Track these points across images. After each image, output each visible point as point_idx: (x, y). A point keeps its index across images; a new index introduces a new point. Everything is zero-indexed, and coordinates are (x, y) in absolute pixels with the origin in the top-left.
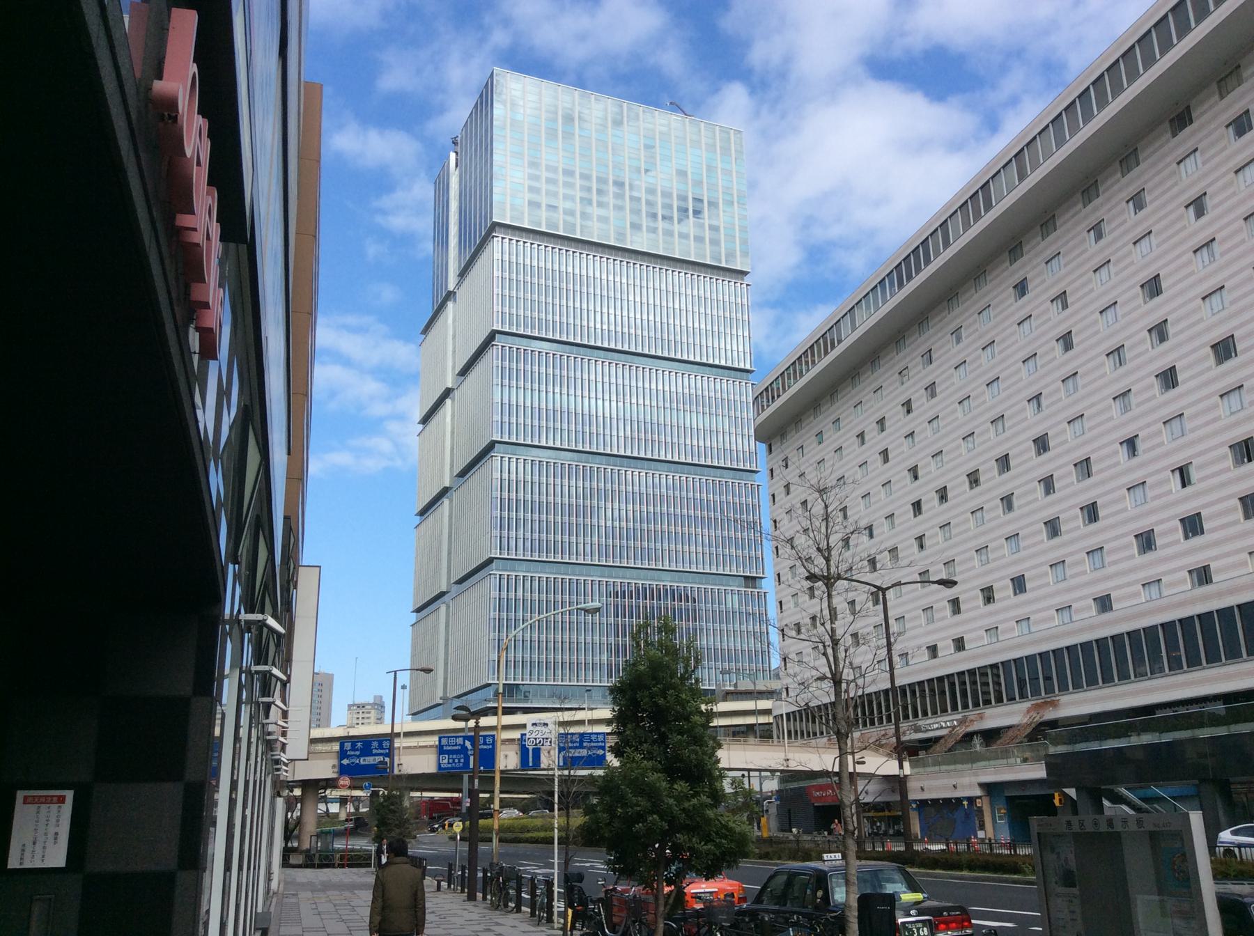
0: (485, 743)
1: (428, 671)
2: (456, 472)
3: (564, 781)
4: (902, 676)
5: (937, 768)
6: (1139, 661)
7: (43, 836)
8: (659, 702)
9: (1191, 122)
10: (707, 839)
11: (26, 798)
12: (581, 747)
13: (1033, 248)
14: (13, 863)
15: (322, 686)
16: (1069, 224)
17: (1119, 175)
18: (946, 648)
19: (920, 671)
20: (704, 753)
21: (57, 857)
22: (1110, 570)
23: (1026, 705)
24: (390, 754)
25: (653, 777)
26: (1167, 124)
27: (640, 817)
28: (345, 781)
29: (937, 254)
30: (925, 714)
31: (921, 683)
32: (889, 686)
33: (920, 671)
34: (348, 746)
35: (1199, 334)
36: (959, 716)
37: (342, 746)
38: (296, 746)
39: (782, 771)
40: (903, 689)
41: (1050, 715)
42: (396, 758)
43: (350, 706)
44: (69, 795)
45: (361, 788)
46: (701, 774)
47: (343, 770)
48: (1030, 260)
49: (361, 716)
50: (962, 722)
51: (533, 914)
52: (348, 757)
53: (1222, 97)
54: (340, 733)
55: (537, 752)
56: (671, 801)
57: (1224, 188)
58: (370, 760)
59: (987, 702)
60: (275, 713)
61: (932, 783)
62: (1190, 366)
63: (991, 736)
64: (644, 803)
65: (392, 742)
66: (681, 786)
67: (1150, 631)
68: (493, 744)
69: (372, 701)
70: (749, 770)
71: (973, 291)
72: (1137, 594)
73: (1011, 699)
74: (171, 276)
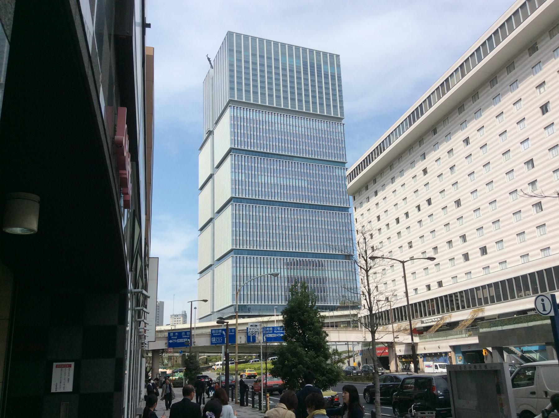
0: (231, 332)
1: (206, 301)
2: (216, 211)
3: (266, 348)
4: (412, 299)
5: (431, 339)
6: (519, 290)
7: (63, 380)
8: (302, 320)
9: (537, 50)
10: (323, 375)
11: (57, 365)
12: (273, 333)
13: (469, 107)
14: (53, 390)
15: (160, 307)
16: (485, 96)
17: (506, 74)
18: (434, 286)
19: (423, 296)
20: (320, 339)
21: (69, 387)
22: (506, 250)
23: (470, 311)
24: (190, 338)
25: (299, 349)
26: (527, 51)
27: (295, 366)
28: (171, 350)
29: (426, 111)
30: (425, 315)
31: (423, 302)
32: (406, 304)
33: (423, 296)
34: (172, 334)
35: (470, 206)
36: (440, 316)
37: (169, 334)
38: (150, 336)
39: (362, 342)
40: (412, 305)
41: (480, 315)
42: (193, 339)
43: (171, 316)
44: (73, 364)
45: (177, 352)
46: (319, 346)
47: (170, 345)
48: (468, 112)
49: (176, 320)
50: (442, 319)
51: (253, 407)
52: (172, 339)
53: (551, 38)
54: (169, 328)
55: (254, 338)
56: (307, 359)
57: (553, 78)
58: (181, 341)
59: (453, 309)
60: (142, 325)
61: (425, 346)
62: (540, 158)
63: (452, 326)
64: (295, 360)
65: (190, 332)
66: (312, 353)
67: (524, 277)
68: (235, 332)
69: (181, 313)
70: (348, 342)
71: (443, 126)
72: (518, 260)
73: (463, 307)
74: (117, 187)
